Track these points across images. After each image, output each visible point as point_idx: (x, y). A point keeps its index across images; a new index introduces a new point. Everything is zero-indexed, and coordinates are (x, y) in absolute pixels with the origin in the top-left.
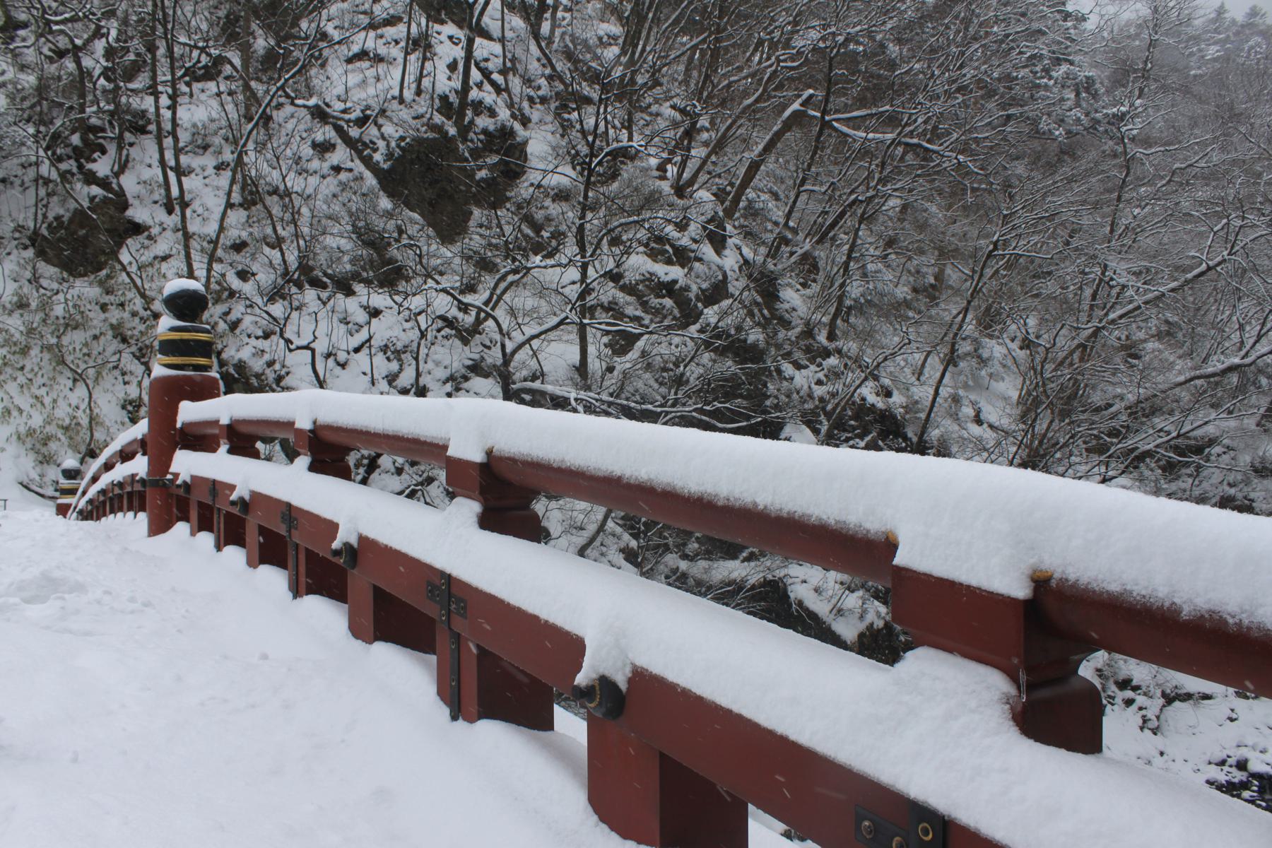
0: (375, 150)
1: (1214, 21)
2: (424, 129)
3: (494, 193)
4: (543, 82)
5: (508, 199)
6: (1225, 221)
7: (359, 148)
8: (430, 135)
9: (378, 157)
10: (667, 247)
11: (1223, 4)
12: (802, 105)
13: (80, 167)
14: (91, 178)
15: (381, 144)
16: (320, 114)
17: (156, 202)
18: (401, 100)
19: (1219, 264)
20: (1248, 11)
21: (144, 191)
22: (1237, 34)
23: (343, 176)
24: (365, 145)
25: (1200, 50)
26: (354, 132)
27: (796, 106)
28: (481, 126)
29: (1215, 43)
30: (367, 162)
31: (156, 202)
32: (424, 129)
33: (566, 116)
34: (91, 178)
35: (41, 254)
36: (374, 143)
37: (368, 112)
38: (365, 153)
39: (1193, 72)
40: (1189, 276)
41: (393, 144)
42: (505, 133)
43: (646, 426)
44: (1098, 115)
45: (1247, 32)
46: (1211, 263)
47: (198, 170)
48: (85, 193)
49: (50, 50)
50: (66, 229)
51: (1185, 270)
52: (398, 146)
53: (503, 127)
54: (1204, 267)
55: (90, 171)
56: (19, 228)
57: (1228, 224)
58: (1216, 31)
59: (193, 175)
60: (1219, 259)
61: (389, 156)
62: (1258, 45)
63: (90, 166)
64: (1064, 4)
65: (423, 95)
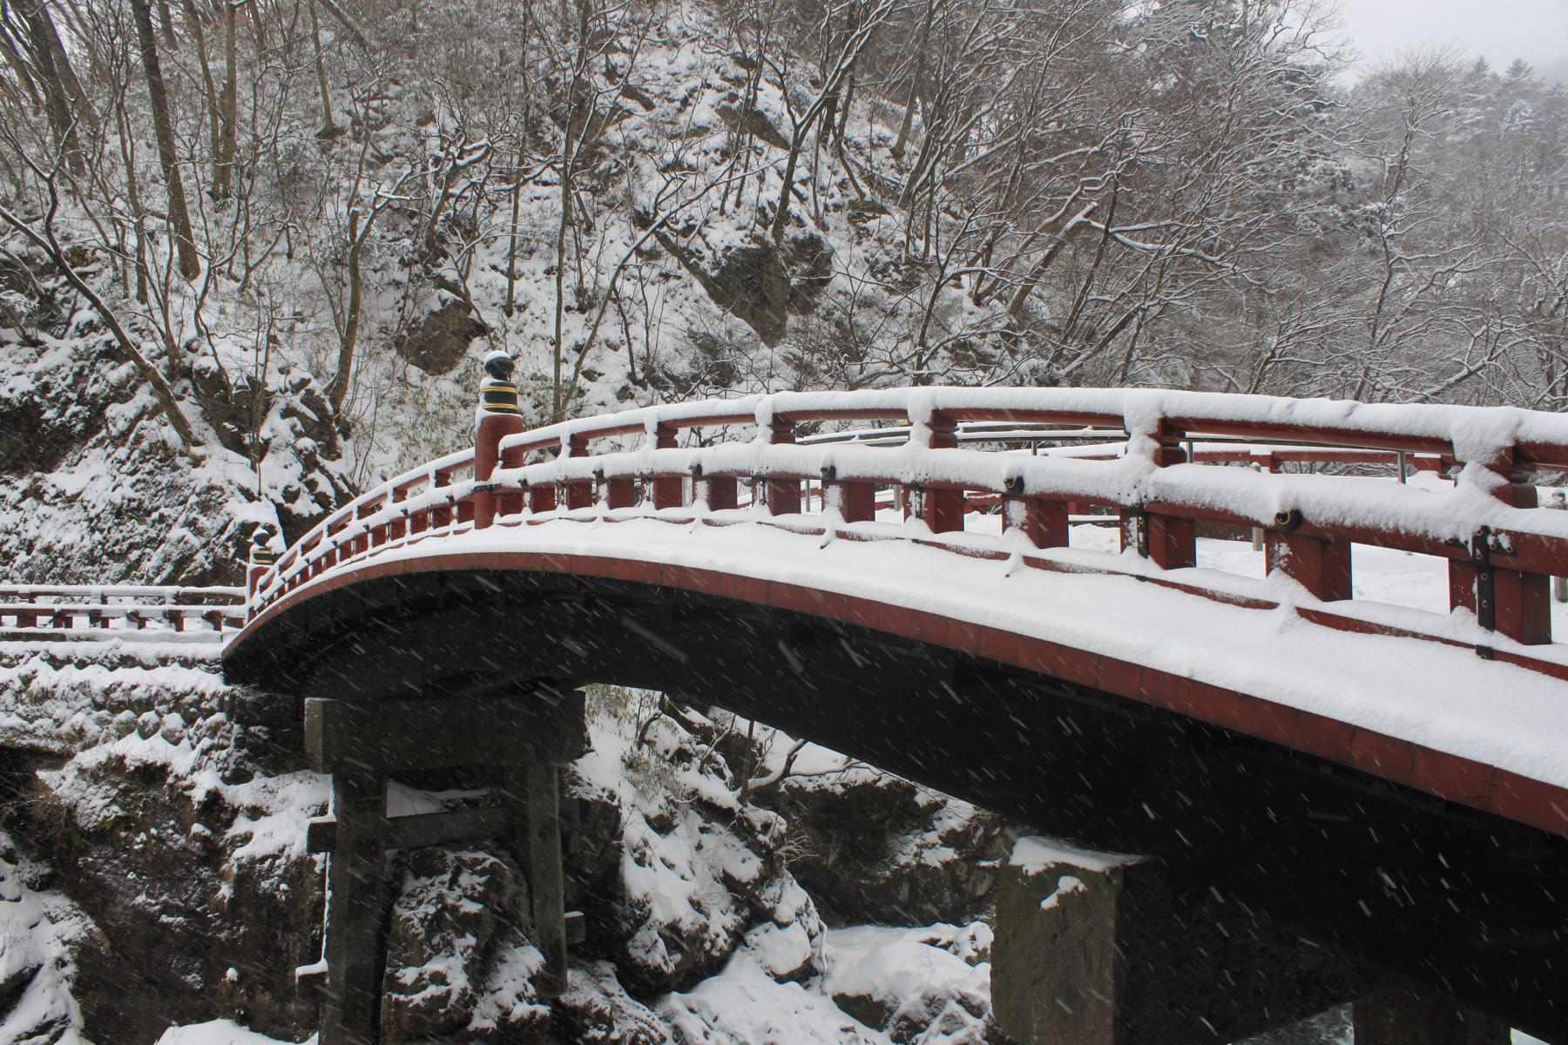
0: (702, 259)
1: (1470, 77)
2: (747, 240)
3: (804, 300)
4: (835, 190)
5: (816, 306)
6: (1485, 327)
7: (685, 256)
8: (754, 246)
9: (705, 265)
10: (970, 353)
11: (1482, 59)
12: (1085, 216)
13: (428, 272)
14: (442, 283)
15: (707, 253)
16: (642, 220)
17: (495, 305)
18: (722, 212)
19: (1479, 369)
20: (1511, 65)
21: (484, 294)
22: (1499, 95)
23: (672, 283)
24: (692, 254)
25: (1458, 114)
26: (683, 242)
27: (1079, 217)
28: (791, 236)
29: (1476, 104)
30: (694, 270)
31: (495, 305)
32: (747, 240)
33: (861, 224)
34: (442, 283)
35: (400, 353)
36: (700, 252)
37: (691, 222)
38: (692, 261)
39: (1449, 138)
40: (1452, 380)
41: (719, 254)
42: (814, 243)
43: (1211, 468)
44: (1356, 212)
45: (1511, 92)
46: (1472, 368)
47: (528, 274)
48: (436, 299)
49: (372, 155)
50: (423, 330)
51: (1445, 373)
52: (724, 256)
53: (812, 236)
54: (1465, 372)
55: (439, 275)
56: (384, 329)
57: (1487, 330)
58: (1476, 90)
59: (523, 278)
60: (1480, 364)
61: (716, 264)
62: (1522, 108)
63: (436, 271)
64: (1563, 600)
65: (742, 207)
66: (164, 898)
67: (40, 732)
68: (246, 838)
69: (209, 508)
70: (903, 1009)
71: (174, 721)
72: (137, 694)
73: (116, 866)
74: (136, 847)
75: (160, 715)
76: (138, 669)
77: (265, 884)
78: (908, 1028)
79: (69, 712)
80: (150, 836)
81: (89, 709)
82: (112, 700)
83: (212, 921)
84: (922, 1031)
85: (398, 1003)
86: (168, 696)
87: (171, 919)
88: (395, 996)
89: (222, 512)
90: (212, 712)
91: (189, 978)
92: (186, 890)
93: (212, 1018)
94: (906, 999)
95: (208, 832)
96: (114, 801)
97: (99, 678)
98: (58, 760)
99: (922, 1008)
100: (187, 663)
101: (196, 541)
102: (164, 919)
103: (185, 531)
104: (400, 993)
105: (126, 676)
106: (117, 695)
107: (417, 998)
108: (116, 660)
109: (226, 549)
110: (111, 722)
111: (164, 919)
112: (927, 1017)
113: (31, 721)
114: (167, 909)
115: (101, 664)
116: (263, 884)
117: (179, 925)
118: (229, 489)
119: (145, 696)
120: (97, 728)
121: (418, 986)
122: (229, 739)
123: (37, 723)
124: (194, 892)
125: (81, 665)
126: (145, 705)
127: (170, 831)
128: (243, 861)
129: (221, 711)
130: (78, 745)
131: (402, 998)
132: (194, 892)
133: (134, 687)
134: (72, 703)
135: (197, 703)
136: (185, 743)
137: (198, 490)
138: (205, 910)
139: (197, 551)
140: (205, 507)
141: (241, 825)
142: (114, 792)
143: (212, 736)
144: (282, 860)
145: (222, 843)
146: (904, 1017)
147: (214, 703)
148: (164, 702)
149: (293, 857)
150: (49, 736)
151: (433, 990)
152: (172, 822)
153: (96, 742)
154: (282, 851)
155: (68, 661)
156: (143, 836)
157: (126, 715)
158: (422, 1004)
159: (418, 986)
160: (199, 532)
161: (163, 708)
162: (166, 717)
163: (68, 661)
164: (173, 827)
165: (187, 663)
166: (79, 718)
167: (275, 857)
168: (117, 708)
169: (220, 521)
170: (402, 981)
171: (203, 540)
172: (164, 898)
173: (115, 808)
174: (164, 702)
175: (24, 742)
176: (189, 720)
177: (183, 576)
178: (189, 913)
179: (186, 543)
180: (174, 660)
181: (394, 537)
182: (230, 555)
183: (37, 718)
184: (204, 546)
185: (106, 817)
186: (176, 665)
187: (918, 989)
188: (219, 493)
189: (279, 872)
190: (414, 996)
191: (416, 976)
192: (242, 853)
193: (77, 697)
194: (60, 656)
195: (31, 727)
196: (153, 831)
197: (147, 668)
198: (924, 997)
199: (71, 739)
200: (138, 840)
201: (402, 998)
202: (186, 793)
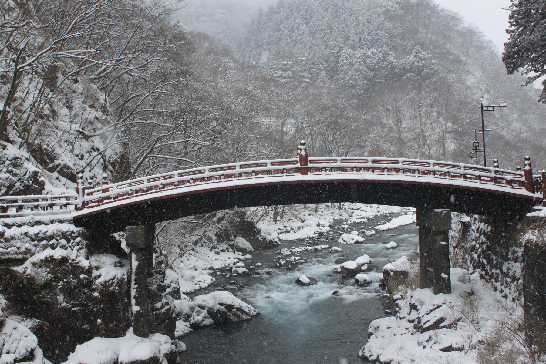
61: (44, 71)
66: (72, 302)
67: (12, 252)
68: (99, 276)
69: (17, 166)
70: (185, 312)
71: (63, 242)
72: (49, 234)
73: (52, 295)
74: (59, 287)
75: (57, 240)
76: (43, 226)
77: (111, 289)
78: (187, 317)
79: (22, 244)
80: (64, 282)
81: (30, 241)
82: (39, 237)
83: (90, 306)
84: (191, 317)
85: (156, 314)
86: (60, 233)
87: (75, 309)
88: (155, 312)
89: (23, 167)
90: (76, 237)
91: (85, 326)
92: (80, 298)
93: (93, 338)
94: (185, 309)
95: (87, 277)
96: (49, 273)
97: (33, 231)
98: (21, 262)
99: (190, 310)
100: (61, 222)
101: (15, 179)
102: (73, 309)
103: (8, 175)
104: (156, 311)
105: (42, 228)
106: (41, 235)
107: (163, 310)
108: (33, 223)
109: (28, 181)
110: (39, 245)
111: (73, 309)
112: (191, 313)
113: (7, 249)
114: (74, 306)
115: (27, 225)
116: (110, 289)
117: (78, 310)
118: (23, 158)
119: (52, 234)
120: (34, 248)
121: (163, 307)
122: (83, 245)
123: (10, 249)
124: (83, 298)
125: (19, 226)
126: (51, 237)
127: (71, 279)
128: (103, 283)
129: (79, 236)
130: (29, 255)
131: (158, 312)
132: (83, 298)
133: (46, 232)
134: (22, 240)
135: (70, 235)
136: (69, 248)
137: (10, 158)
138: (87, 303)
139: (16, 182)
140: (15, 165)
141: (95, 273)
142: (48, 269)
143: (78, 245)
144: (116, 280)
145: (91, 279)
146: (186, 314)
147: (76, 234)
148: (59, 235)
149: (119, 278)
150: (16, 253)
151: (167, 307)
152: (71, 276)
153: (35, 253)
154: (115, 277)
155: (13, 225)
156: (61, 283)
157: (45, 242)
158: (165, 312)
159: (163, 307)
160: (15, 175)
161: (58, 238)
162: (60, 241)
163: (13, 225)
164: (72, 277)
165: (61, 222)
166: (27, 245)
167: (113, 280)
168: (43, 239)
169: (23, 171)
170: (157, 307)
171: (18, 178)
172: (72, 302)
173: (50, 275)
174: (59, 235)
175: (6, 257)
176: (69, 241)
177: (11, 192)
178: (81, 305)
179: (11, 179)
180: (56, 221)
181: (413, 173)
182: (31, 184)
183: (9, 247)
184: (18, 180)
185: (47, 279)
186: (57, 223)
187: (187, 306)
188: (20, 160)
189: (115, 284)
190: (162, 310)
191: (161, 304)
192: (98, 281)
193: (24, 237)
194: (11, 223)
195: (8, 251)
196: (65, 280)
197: (47, 224)
198: (189, 307)
199: (26, 253)
200: (60, 284)
201: (158, 312)
202: (77, 265)
